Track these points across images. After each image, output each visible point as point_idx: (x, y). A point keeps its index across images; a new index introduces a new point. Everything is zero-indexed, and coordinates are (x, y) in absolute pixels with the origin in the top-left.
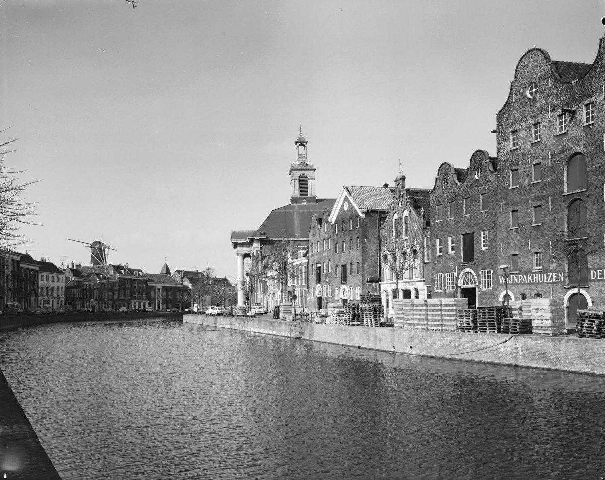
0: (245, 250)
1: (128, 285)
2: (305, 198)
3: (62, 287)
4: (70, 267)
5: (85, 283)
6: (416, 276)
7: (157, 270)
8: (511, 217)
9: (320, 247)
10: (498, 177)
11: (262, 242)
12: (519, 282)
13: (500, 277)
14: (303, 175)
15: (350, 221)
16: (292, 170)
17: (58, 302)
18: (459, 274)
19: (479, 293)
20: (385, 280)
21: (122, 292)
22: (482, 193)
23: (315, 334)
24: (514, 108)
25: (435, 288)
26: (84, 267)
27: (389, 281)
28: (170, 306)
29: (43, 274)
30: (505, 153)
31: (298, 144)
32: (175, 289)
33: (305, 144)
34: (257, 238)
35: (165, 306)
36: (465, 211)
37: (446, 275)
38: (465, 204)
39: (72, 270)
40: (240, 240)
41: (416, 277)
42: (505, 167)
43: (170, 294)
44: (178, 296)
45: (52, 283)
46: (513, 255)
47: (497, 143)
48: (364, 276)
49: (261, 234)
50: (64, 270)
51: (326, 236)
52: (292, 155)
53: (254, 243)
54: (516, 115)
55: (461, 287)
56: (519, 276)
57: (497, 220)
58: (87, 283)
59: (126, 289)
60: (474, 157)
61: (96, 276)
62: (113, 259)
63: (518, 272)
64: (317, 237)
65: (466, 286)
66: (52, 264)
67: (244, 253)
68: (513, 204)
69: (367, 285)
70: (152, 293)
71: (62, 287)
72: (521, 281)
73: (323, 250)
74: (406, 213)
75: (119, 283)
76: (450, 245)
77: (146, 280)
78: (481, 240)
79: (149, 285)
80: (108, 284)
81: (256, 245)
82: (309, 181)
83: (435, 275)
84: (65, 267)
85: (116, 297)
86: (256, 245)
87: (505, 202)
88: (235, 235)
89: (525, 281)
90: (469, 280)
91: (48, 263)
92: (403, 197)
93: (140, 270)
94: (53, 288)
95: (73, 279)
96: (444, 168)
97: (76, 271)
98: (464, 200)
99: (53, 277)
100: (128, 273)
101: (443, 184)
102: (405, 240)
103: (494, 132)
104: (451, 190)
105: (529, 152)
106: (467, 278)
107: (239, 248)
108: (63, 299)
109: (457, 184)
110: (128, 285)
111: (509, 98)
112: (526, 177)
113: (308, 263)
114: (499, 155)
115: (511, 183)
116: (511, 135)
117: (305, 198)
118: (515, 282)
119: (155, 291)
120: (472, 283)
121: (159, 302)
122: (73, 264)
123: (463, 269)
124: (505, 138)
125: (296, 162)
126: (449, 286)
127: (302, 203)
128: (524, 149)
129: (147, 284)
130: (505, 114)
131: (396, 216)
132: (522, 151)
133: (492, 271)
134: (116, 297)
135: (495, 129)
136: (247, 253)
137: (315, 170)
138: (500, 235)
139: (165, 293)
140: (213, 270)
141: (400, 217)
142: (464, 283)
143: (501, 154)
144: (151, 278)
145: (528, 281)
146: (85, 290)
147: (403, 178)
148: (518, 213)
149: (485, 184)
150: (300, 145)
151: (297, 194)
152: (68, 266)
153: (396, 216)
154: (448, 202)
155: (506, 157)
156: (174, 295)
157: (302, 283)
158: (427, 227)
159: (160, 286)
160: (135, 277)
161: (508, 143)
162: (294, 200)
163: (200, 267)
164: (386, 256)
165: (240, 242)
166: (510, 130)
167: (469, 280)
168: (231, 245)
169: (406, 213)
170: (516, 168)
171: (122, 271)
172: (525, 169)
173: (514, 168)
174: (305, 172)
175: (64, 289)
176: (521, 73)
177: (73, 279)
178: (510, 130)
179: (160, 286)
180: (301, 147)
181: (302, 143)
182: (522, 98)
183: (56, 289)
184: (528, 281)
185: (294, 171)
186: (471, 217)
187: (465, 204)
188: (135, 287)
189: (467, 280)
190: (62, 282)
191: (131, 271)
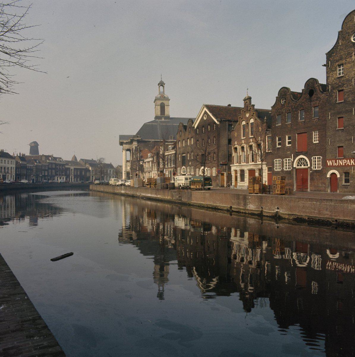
0: (127, 146)
1: (54, 166)
2: (163, 117)
3: (14, 168)
4: (19, 155)
5: (27, 165)
6: (243, 162)
7: (70, 159)
8: (338, 121)
9: (185, 144)
10: (327, 95)
11: (138, 141)
12: (344, 165)
13: (328, 161)
14: (162, 103)
15: (208, 127)
16: (156, 100)
17: (11, 176)
18: (294, 160)
19: (311, 172)
20: (235, 163)
21: (50, 171)
22: (314, 106)
23: (193, 198)
24: (341, 49)
25: (275, 168)
26: (27, 156)
27: (245, 164)
28: (79, 179)
29: (5, 159)
30: (333, 79)
31: (160, 85)
32: (81, 170)
33: (163, 85)
34: (136, 139)
35: (75, 179)
36: (299, 118)
37: (284, 160)
38: (299, 113)
39: (20, 157)
40: (124, 140)
41: (242, 163)
42: (333, 88)
43: (79, 173)
44: (83, 174)
45: (8, 164)
46: (339, 147)
47: (327, 73)
48: (218, 162)
49: (138, 137)
50: (15, 157)
51: (190, 136)
52: (156, 92)
53: (134, 143)
54: (342, 54)
55: (295, 168)
56: (344, 160)
57: (326, 124)
58: (30, 165)
59: (52, 169)
60: (307, 83)
61: (34, 161)
62: (43, 151)
63: (343, 158)
64: (183, 137)
65: (299, 167)
66: (8, 153)
67: (126, 148)
68: (339, 113)
69: (220, 167)
70: (68, 172)
71: (14, 168)
72: (345, 164)
73: (187, 145)
74: (252, 121)
75: (48, 166)
76: (287, 141)
77: (64, 164)
78: (312, 137)
79: (66, 167)
80: (41, 166)
81: (135, 144)
82: (166, 107)
83: (312, 158)
84: (16, 155)
85: (46, 174)
86: (135, 144)
87: (332, 112)
88: (121, 137)
89: (348, 164)
90: (302, 163)
91: (6, 153)
92: (250, 110)
93: (60, 158)
94: (8, 168)
95: (20, 163)
96: (284, 93)
97: (23, 158)
98: (299, 111)
99: (8, 161)
100: (53, 160)
101: (282, 101)
102: (251, 138)
103: (325, 65)
104: (289, 104)
105: (352, 78)
106: (300, 162)
107: (124, 146)
108: (14, 175)
109: (293, 101)
110: (54, 166)
111: (336, 43)
112: (350, 95)
113: (176, 154)
114: (328, 81)
115: (338, 99)
116: (338, 67)
117: (163, 117)
118: (340, 164)
119: (70, 170)
120: (305, 165)
121: (72, 177)
122: (20, 154)
123: (297, 156)
124: (333, 69)
125: (158, 95)
126: (276, 167)
127: (162, 119)
128: (348, 76)
129: (65, 166)
130: (333, 53)
131: (244, 123)
132: (347, 78)
133: (321, 157)
134: (46, 174)
135: (325, 64)
136: (129, 148)
137: (169, 100)
138: (328, 134)
139: (76, 172)
140: (104, 159)
141: (247, 123)
142: (298, 165)
143: (330, 80)
144: (68, 163)
145: (350, 164)
146: (27, 169)
147: (250, 98)
148: (344, 119)
149: (317, 100)
150: (160, 86)
151: (159, 114)
152: (17, 155)
153: (244, 123)
154: (286, 112)
155: (334, 82)
156: (81, 173)
157: (171, 165)
158: (268, 130)
159: (72, 168)
160: (58, 162)
161: (335, 73)
162: (157, 117)
163: (95, 157)
164: (236, 149)
165: (125, 142)
166: (337, 64)
167: (302, 163)
168: (118, 143)
169: (252, 121)
170: (342, 89)
171: (50, 158)
172: (349, 90)
173: (340, 89)
174: (164, 102)
175: (15, 168)
176: (347, 26)
177: (20, 163)
178: (337, 64)
179: (72, 168)
180: (161, 87)
181: (162, 84)
182: (347, 43)
183: (10, 169)
184: (350, 164)
185: (157, 101)
186: (304, 122)
187: (299, 113)
188: (58, 168)
189: (300, 163)
190: (14, 164)
191: (55, 159)
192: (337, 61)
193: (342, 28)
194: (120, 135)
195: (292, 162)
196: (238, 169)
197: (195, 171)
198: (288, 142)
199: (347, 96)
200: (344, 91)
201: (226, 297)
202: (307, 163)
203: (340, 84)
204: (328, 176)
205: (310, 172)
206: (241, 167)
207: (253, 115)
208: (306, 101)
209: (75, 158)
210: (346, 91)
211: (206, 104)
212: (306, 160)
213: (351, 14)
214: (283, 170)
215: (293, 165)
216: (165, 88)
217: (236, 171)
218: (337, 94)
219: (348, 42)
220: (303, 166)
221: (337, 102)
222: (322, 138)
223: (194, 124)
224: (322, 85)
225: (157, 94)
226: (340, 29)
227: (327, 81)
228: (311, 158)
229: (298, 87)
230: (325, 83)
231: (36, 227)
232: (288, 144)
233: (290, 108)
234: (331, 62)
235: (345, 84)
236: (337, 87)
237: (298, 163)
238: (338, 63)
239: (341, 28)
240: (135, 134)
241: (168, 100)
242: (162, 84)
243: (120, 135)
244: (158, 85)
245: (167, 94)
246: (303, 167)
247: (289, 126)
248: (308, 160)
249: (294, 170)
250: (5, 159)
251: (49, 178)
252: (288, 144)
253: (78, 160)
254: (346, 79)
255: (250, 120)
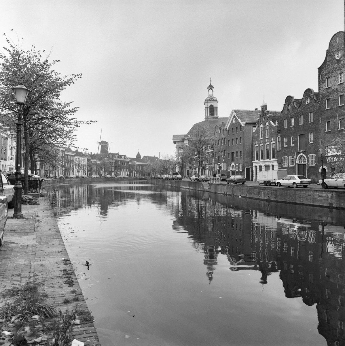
4: (90, 153)
18: (296, 157)
31: (209, 89)
37: (289, 157)
42: (323, 97)
43: (141, 169)
52: (206, 94)
62: (112, 150)
65: (300, 163)
76: (292, 141)
77: (128, 161)
90: (302, 160)
93: (125, 156)
120: (304, 162)
128: (334, 87)
142: (299, 162)
144: (132, 159)
149: (312, 107)
150: (210, 89)
181: (211, 87)
191: (121, 156)
192: (326, 75)
193: (329, 48)
194: (174, 136)
195: (295, 159)
196: (258, 165)
197: (227, 167)
198: (293, 142)
199: (333, 104)
200: (331, 100)
201: (291, 299)
202: (305, 160)
203: (328, 94)
204: (320, 171)
205: (307, 167)
206: (259, 164)
207: (268, 119)
208: (304, 108)
209: (138, 155)
210: (332, 99)
211: (236, 109)
212: (305, 158)
213: (335, 36)
214: (289, 166)
215: (295, 161)
216: (213, 91)
217: (256, 167)
218: (326, 102)
219: (334, 59)
220: (303, 162)
221: (326, 109)
222: (315, 139)
223: (226, 126)
224: (316, 94)
225: (206, 96)
226: (328, 48)
227: (319, 90)
228: (308, 156)
229: (299, 95)
230: (318, 92)
231: (106, 216)
232: (293, 144)
233: (293, 114)
234: (321, 75)
235: (331, 94)
236: (325, 97)
237: (300, 160)
238: (326, 76)
239: (328, 48)
240: (186, 134)
241: (216, 101)
242: (211, 87)
243: (174, 136)
244: (208, 88)
245: (216, 95)
246: (303, 163)
247: (293, 129)
248: (306, 157)
249: (297, 166)
250: (84, 158)
251: (115, 173)
252: (293, 144)
253: (142, 157)
254: (332, 90)
255: (266, 124)
